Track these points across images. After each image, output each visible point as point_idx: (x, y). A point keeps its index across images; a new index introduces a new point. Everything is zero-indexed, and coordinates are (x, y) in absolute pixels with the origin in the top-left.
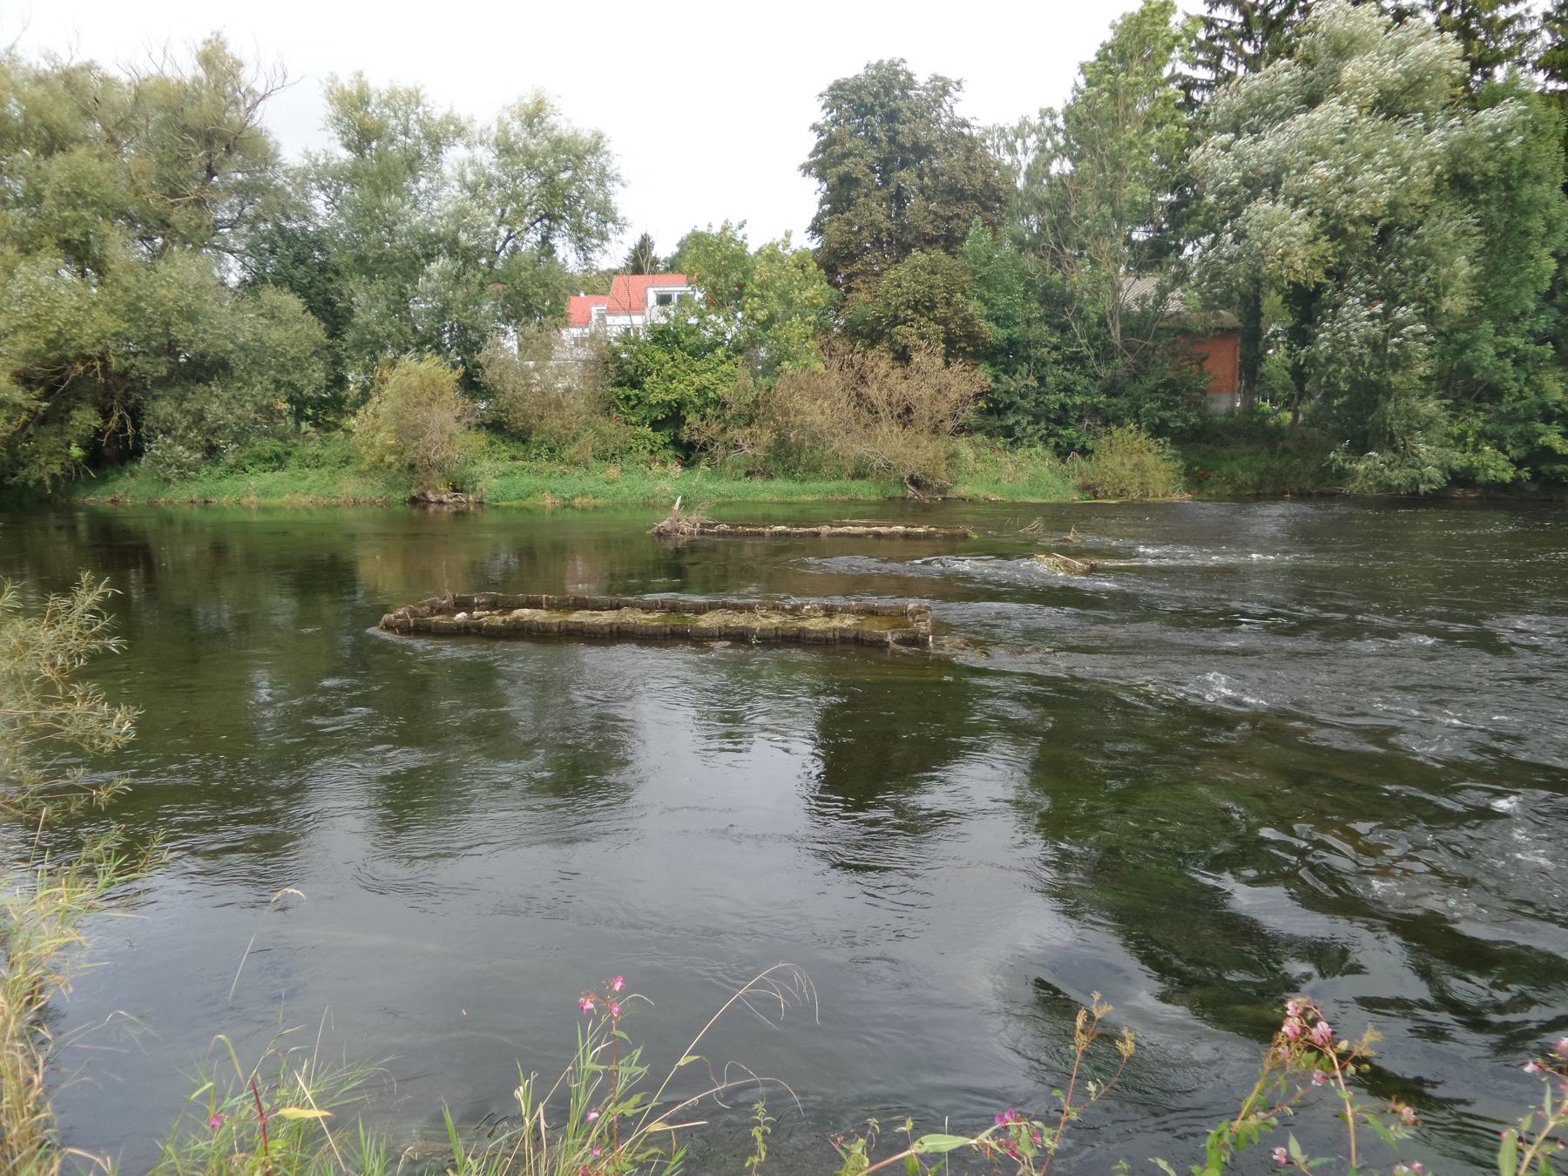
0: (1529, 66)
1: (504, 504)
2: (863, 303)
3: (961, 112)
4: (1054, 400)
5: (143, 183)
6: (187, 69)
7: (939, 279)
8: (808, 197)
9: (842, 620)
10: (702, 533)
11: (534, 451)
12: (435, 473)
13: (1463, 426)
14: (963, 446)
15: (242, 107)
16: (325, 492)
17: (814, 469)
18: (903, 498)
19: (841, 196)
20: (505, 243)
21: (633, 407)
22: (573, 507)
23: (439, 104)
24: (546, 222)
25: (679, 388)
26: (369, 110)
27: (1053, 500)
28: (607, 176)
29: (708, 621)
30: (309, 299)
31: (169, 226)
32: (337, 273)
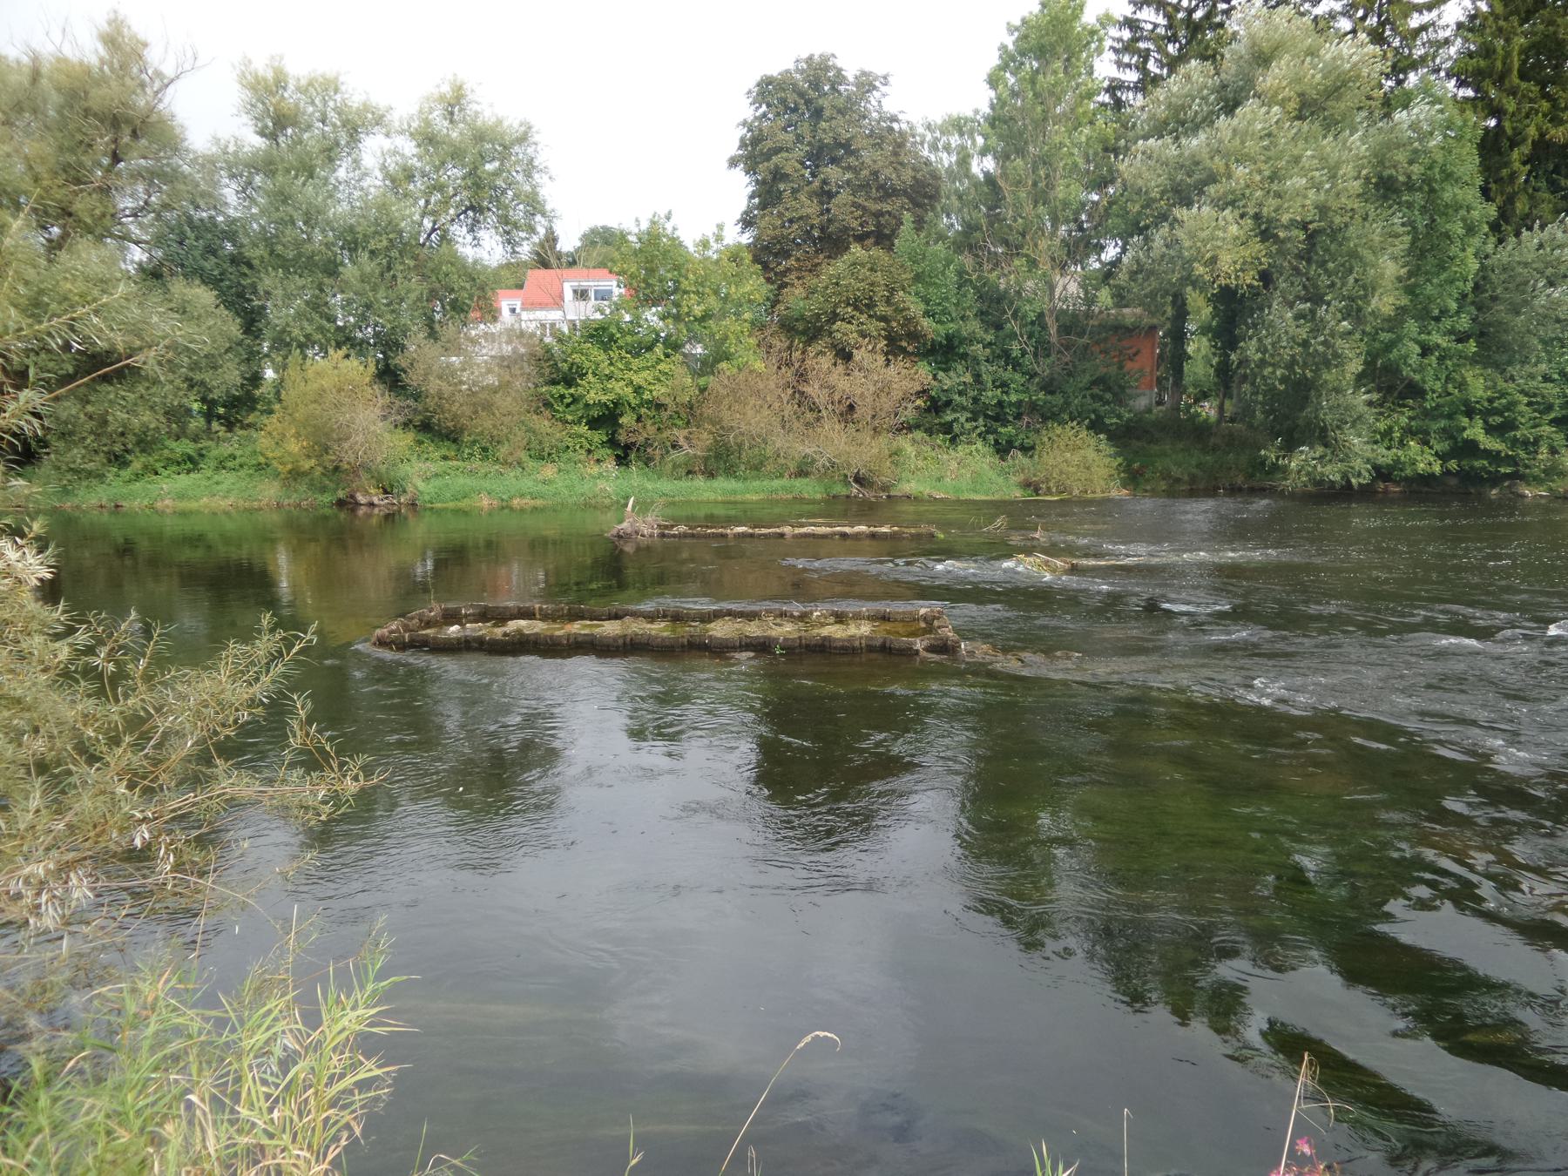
0: (1442, 74)
1: (439, 505)
2: (796, 298)
3: (890, 107)
4: (991, 396)
5: (40, 169)
6: (86, 49)
7: (879, 277)
8: (738, 190)
9: (858, 627)
10: (663, 535)
11: (467, 451)
12: (364, 476)
13: (1388, 422)
14: (905, 443)
15: (148, 90)
16: (246, 495)
17: (757, 467)
18: (848, 497)
19: (768, 194)
20: (429, 235)
21: (568, 405)
22: (511, 509)
23: (357, 92)
24: (470, 213)
25: (620, 388)
26: (286, 95)
27: (997, 497)
28: (534, 167)
29: (721, 630)
30: (222, 293)
31: (70, 215)
32: (250, 266)
